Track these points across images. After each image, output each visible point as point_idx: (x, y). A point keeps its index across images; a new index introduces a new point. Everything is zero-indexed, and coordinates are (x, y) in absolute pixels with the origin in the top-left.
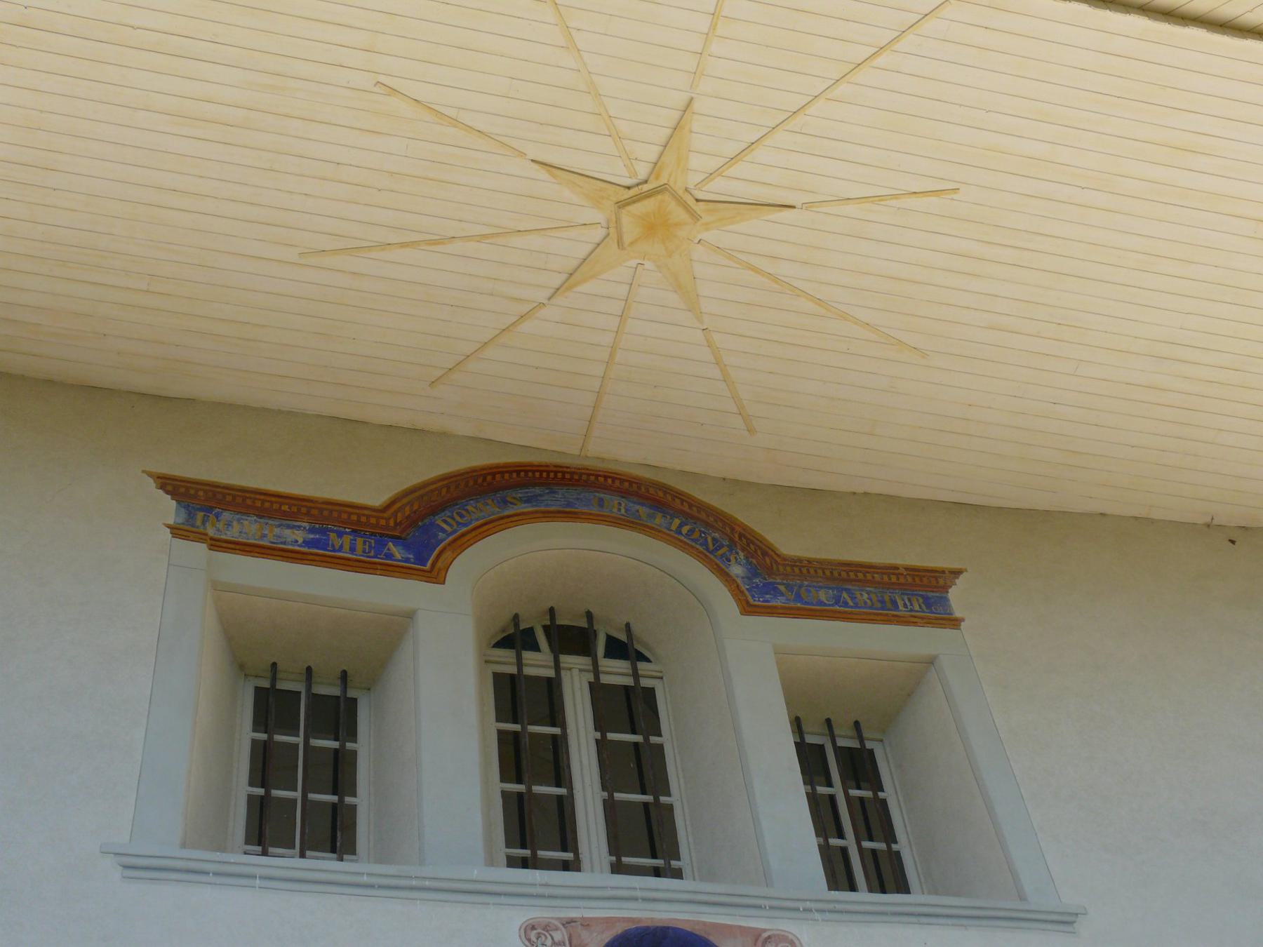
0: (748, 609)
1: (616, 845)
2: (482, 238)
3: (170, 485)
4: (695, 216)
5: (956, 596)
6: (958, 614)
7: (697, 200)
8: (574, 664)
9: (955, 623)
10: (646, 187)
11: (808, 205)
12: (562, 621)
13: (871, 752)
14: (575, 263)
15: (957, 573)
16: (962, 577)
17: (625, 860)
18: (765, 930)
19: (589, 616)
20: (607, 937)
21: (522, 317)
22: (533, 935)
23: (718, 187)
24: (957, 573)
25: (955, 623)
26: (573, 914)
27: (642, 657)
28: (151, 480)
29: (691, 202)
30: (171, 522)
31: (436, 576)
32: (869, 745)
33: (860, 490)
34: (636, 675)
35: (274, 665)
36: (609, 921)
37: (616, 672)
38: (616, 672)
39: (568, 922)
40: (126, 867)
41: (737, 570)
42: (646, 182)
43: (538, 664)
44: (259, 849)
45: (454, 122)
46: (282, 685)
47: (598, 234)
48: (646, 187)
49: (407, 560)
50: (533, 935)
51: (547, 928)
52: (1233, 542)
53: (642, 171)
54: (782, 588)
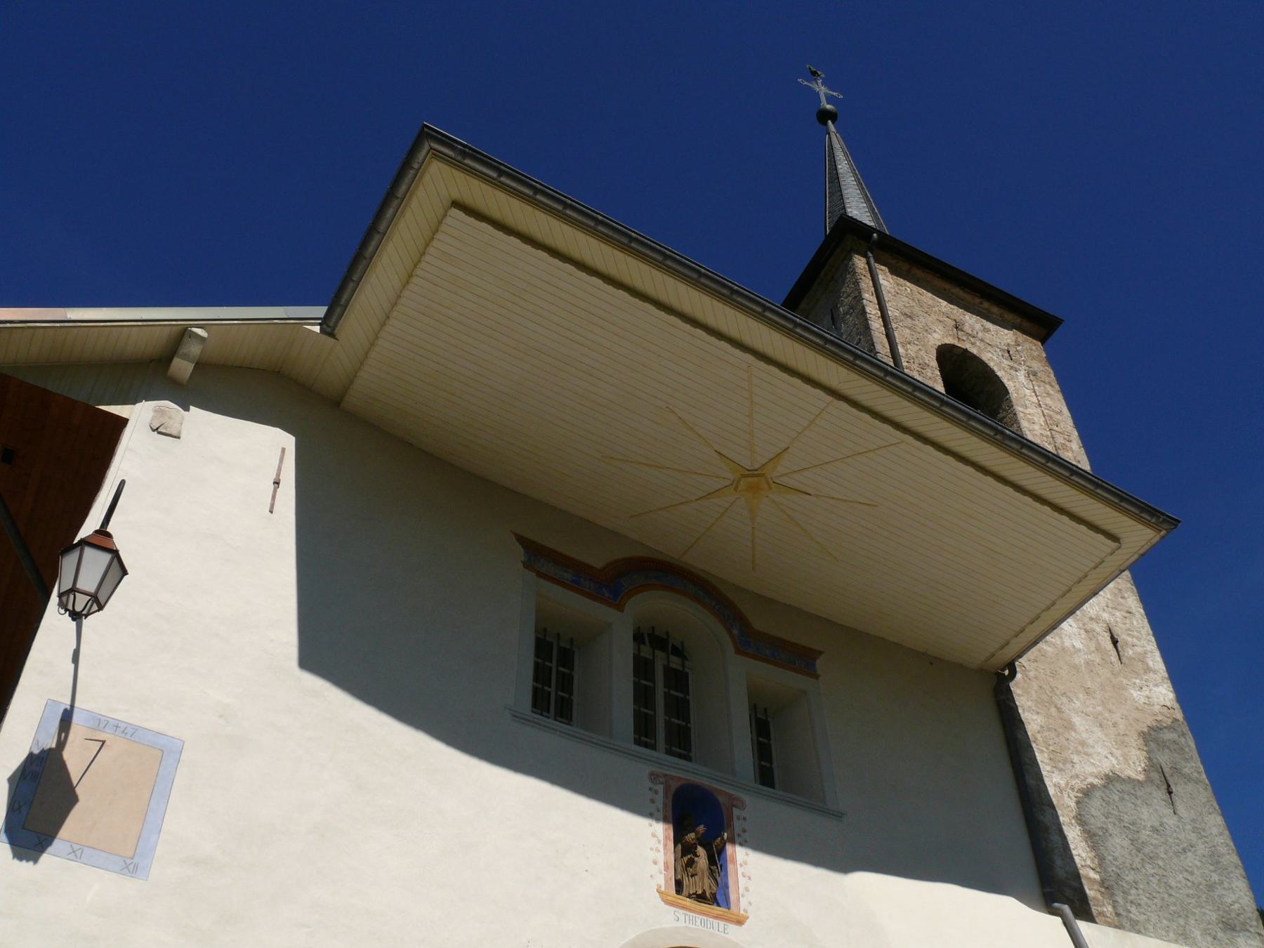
0: (738, 652)
1: (669, 741)
2: (679, 471)
3: (521, 540)
4: (770, 488)
5: (819, 663)
6: (819, 672)
7: (774, 482)
8: (659, 654)
9: (816, 677)
10: (756, 472)
11: (817, 496)
12: (657, 633)
13: (687, 673)
14: (713, 490)
15: (821, 653)
16: (823, 655)
17: (674, 748)
18: (733, 795)
19: (667, 633)
20: (679, 784)
21: (682, 503)
22: (653, 777)
23: (784, 480)
24: (821, 653)
25: (816, 677)
26: (667, 772)
27: (687, 659)
28: (514, 537)
29: (771, 481)
30: (523, 560)
31: (620, 608)
32: (687, 670)
33: (788, 603)
34: (683, 666)
35: (572, 639)
36: (679, 779)
37: (675, 662)
38: (675, 662)
39: (665, 775)
40: (514, 716)
41: (735, 632)
42: (756, 470)
43: (646, 651)
44: (539, 711)
45: (691, 429)
46: (548, 639)
47: (728, 483)
48: (756, 472)
49: (609, 598)
50: (653, 777)
51: (658, 776)
52: (931, 664)
53: (757, 466)
54: (752, 644)
